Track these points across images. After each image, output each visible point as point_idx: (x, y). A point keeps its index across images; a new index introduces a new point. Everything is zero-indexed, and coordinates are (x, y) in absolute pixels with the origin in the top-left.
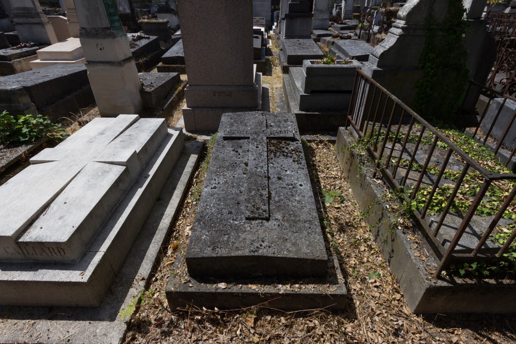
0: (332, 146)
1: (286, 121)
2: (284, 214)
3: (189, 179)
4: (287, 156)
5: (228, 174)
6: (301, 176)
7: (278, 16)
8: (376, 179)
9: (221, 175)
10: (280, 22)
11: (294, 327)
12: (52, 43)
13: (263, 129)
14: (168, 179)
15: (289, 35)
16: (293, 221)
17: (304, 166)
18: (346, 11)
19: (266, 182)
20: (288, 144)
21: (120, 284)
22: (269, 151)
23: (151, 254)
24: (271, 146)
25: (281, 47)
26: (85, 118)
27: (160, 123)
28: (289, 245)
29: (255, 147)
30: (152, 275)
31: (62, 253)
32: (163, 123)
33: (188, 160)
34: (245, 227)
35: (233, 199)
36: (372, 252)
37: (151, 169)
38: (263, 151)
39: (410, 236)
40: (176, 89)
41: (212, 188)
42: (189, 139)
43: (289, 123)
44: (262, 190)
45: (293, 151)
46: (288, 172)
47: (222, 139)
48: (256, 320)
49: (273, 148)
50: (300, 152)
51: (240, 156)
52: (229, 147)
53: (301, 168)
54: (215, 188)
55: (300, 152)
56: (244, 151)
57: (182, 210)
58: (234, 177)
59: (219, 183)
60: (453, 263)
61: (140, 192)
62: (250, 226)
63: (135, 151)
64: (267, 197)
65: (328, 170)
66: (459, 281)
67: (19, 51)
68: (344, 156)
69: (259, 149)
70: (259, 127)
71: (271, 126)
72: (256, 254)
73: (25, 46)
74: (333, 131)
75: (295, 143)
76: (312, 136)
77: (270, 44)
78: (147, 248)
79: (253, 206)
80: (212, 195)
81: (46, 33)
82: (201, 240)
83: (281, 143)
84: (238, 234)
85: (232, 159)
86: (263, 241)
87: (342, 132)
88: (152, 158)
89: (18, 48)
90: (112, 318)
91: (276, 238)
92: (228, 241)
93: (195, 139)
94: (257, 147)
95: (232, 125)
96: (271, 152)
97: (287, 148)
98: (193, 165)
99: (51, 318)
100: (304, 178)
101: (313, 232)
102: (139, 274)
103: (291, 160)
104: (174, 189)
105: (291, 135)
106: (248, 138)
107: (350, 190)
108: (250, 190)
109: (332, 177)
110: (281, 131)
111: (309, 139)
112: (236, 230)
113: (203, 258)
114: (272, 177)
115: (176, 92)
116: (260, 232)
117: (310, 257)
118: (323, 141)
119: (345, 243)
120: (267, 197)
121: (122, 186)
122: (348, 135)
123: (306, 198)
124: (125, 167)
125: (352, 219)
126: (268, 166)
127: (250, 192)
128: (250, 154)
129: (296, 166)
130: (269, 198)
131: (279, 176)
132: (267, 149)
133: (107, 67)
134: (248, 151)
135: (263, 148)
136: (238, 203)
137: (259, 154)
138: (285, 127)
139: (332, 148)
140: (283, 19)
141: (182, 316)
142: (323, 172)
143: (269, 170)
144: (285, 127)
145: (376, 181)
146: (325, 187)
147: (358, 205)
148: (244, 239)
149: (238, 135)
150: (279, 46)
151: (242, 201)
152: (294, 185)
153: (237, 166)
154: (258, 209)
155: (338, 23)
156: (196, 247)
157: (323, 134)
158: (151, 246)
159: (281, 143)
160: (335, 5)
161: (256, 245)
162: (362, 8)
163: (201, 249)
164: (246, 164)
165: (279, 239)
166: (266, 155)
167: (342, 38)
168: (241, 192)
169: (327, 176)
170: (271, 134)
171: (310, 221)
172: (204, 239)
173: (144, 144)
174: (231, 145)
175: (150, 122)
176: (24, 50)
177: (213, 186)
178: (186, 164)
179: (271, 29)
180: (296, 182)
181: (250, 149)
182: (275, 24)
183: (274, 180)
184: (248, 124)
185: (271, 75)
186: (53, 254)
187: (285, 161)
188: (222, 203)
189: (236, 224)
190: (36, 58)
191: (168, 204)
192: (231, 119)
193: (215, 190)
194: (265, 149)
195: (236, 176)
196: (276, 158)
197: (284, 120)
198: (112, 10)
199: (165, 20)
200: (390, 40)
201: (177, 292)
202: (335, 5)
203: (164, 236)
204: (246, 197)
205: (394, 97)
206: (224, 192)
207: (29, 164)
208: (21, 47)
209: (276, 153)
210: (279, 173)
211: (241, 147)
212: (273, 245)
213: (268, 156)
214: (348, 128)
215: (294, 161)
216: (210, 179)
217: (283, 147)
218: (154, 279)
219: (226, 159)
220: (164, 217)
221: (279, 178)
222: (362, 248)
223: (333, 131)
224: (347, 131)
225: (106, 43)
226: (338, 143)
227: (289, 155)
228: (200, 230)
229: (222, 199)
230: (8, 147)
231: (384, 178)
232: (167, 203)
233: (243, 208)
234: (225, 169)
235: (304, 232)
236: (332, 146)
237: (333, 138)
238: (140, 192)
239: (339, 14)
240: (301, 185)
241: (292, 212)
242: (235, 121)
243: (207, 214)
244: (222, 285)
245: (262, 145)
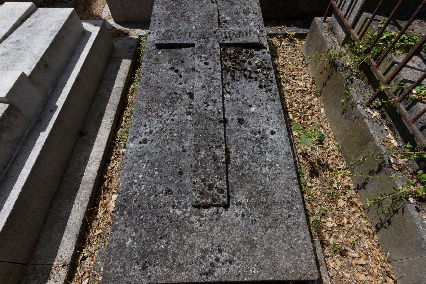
0: (298, 42)
1: (246, 12)
2: (250, 191)
3: (121, 99)
4: (250, 77)
5: (164, 114)
6: (273, 115)
8: (371, 109)
9: (153, 117)
14: (93, 100)
17: (275, 94)
19: (222, 131)
20: (252, 55)
21: (33, 276)
22: (225, 70)
23: (74, 223)
24: (226, 60)
27: (66, 17)
28: (259, 254)
29: (202, 64)
30: (76, 255)
32: (71, 16)
33: (118, 68)
34: (192, 222)
35: (173, 163)
36: (353, 209)
37: (59, 95)
38: (215, 70)
41: (140, 143)
43: (251, 16)
44: (217, 147)
45: (259, 67)
46: (253, 109)
47: (154, 47)
49: (229, 63)
50: (269, 69)
51: (180, 80)
53: (271, 99)
54: (145, 141)
55: (269, 69)
56: (187, 71)
57: (114, 145)
58: (173, 120)
59: (151, 132)
61: (43, 136)
62: (199, 220)
63: (23, 75)
64: (224, 163)
65: (294, 79)
69: (209, 66)
70: (208, 25)
71: (225, 22)
72: (210, 279)
75: (260, 52)
76: (273, 27)
78: (69, 213)
79: (204, 181)
80: (141, 156)
82: (125, 248)
83: (241, 53)
84: (181, 235)
85: (170, 85)
86: (220, 251)
87: (320, 26)
88: (61, 76)
91: (240, 242)
92: (166, 251)
93: (127, 34)
94: (206, 64)
95: (168, 20)
96: (228, 71)
97: (250, 63)
98: (126, 76)
100: (276, 119)
101: (294, 224)
102: (58, 257)
103: (255, 85)
104: (102, 115)
105: (256, 41)
106: (193, 45)
107: (322, 110)
108: (197, 149)
109: (300, 90)
110: (240, 32)
111: (271, 32)
112: (178, 227)
114: (229, 118)
116: (216, 230)
118: (289, 35)
119: (319, 193)
120: (224, 163)
122: (328, 33)
123: (282, 157)
124: (7, 105)
125: (326, 154)
126: (223, 99)
127: (198, 152)
128: (195, 75)
129: (263, 95)
130: (227, 162)
131: (241, 117)
132: (222, 65)
134: (193, 69)
135: (215, 65)
136: (181, 173)
137: (209, 76)
138: (246, 24)
139: (299, 44)
142: (288, 82)
143: (226, 106)
144: (246, 24)
145: (372, 113)
146: (292, 106)
147: (332, 133)
148: (192, 247)
149: (178, 41)
151: (186, 167)
152: (262, 133)
153: (178, 99)
154: (211, 187)
156: (116, 263)
157: (288, 25)
158: (73, 210)
159: (241, 53)
161: (210, 259)
163: (124, 267)
164: (191, 95)
165: (245, 243)
166: (220, 78)
168: (184, 151)
169: (293, 87)
170: (227, 37)
171: (288, 202)
172: (130, 247)
173: (39, 58)
174: (168, 58)
175: (50, 16)
177: (141, 139)
178: (116, 75)
180: (265, 126)
181: (197, 68)
183: (233, 124)
184: (192, 20)
188: (156, 173)
189: (178, 216)
191: (94, 141)
192: (167, 8)
193: (145, 146)
194: (219, 67)
195: (176, 118)
196: (235, 83)
197: (244, 10)
203: (90, 192)
206: (158, 150)
209: (234, 72)
210: (240, 112)
211: (183, 62)
212: (235, 258)
213: (222, 79)
214: (329, 18)
215: (261, 87)
216: (139, 125)
217: (244, 61)
218: (81, 257)
219: (160, 85)
220: (90, 162)
222: (341, 203)
224: (326, 24)
226: (309, 40)
227: (254, 75)
228: (123, 226)
229: (156, 164)
231: (383, 109)
232: (94, 138)
233: (187, 182)
234: (160, 105)
235: (282, 225)
236: (298, 42)
237: (301, 31)
238: (43, 136)
240: (273, 133)
241: (261, 188)
242: (173, 13)
243: (134, 194)
245: (214, 60)
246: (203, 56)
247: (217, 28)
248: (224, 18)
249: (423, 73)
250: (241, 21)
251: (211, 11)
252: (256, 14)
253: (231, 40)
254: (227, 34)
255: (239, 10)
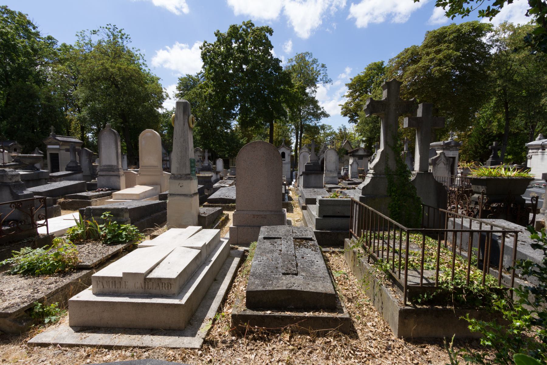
7: (296, 175)
10: (299, 178)
11: (316, 342)
12: (121, 188)
15: (306, 186)
16: (313, 277)
18: (352, 173)
25: (300, 195)
26: (155, 233)
31: (169, 288)
39: (390, 288)
40: (220, 218)
42: (232, 248)
46: (309, 255)
48: (291, 337)
52: (267, 243)
60: (412, 293)
66: (419, 307)
67: (97, 193)
68: (349, 254)
73: (102, 190)
74: (341, 244)
77: (291, 194)
81: (119, 182)
89: (96, 192)
90: (193, 335)
93: (237, 248)
99: (153, 335)
104: (225, 275)
106: (281, 238)
113: (257, 291)
115: (221, 220)
117: (324, 292)
121: (198, 262)
128: (282, 245)
129: (314, 252)
133: (182, 198)
135: (291, 243)
140: (301, 175)
141: (239, 336)
150: (298, 194)
155: (346, 180)
160: (342, 168)
162: (365, 171)
167: (348, 189)
176: (101, 193)
179: (290, 184)
182: (294, 180)
185: (292, 212)
186: (164, 288)
187: (306, 250)
190: (111, 198)
198: (193, 165)
199: (210, 175)
200: (367, 181)
201: (239, 315)
202: (342, 168)
204: (282, 264)
205: (370, 208)
207: (137, 248)
208: (99, 191)
221: (303, 258)
223: (341, 244)
225: (185, 183)
230: (110, 245)
237: (341, 250)
239: (346, 174)
244: (269, 312)
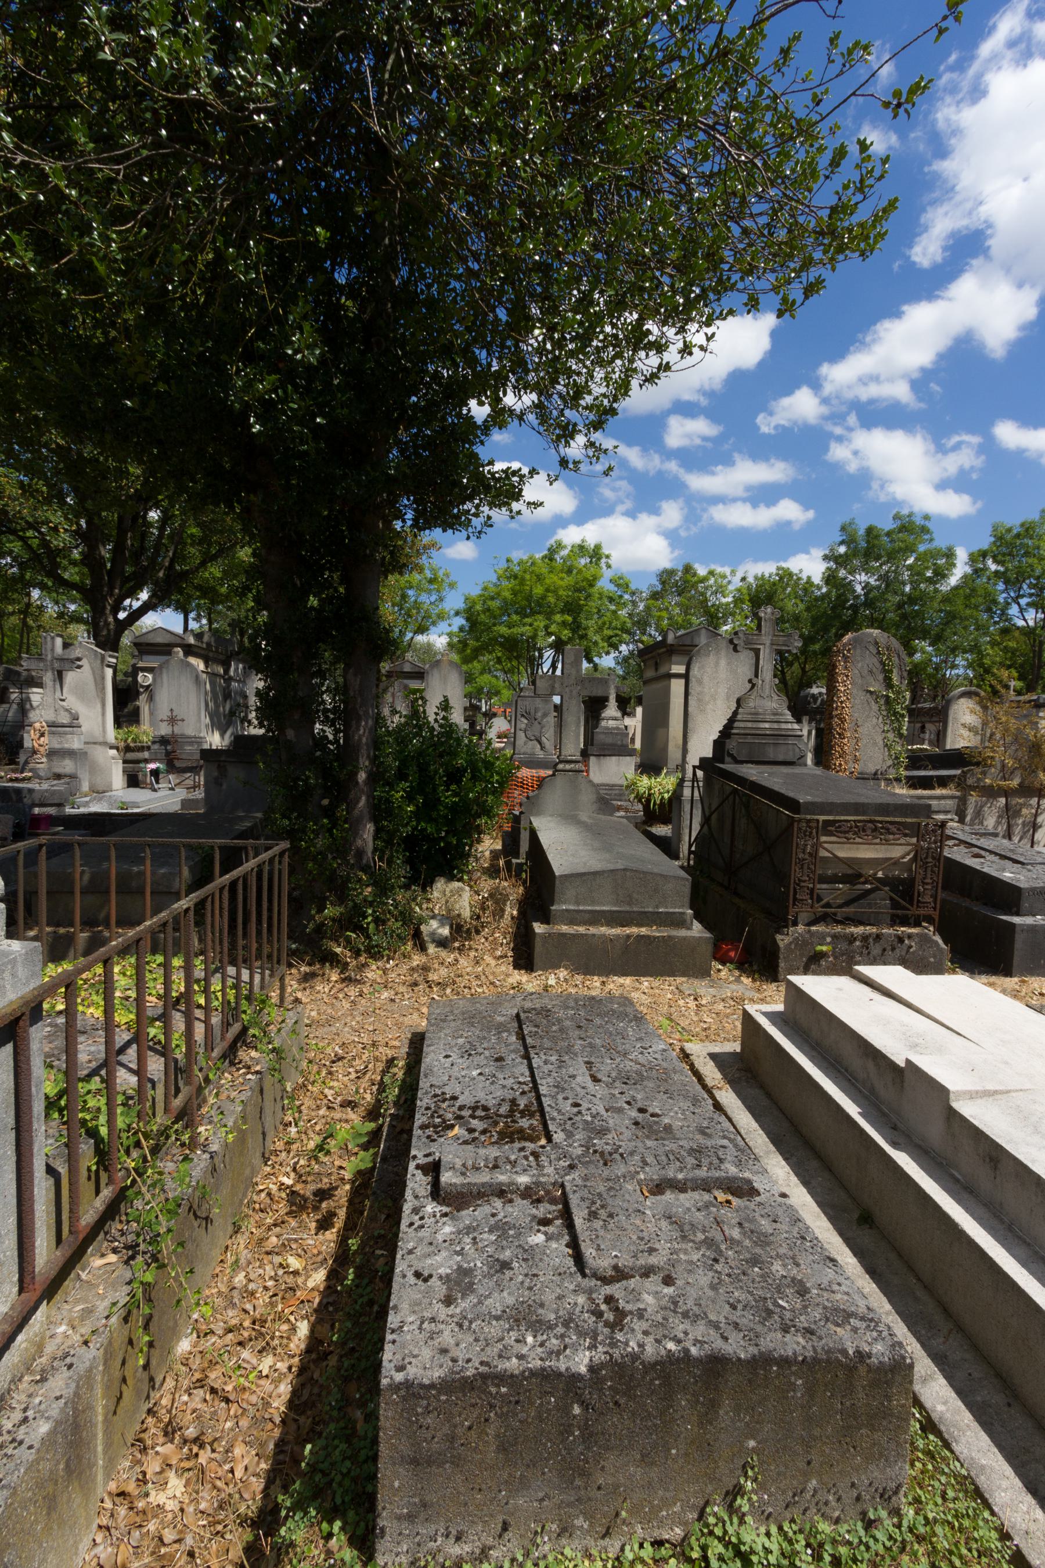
13: (575, 1175)
46: (475, 1073)
61: (852, 1109)
69: (570, 1101)
94: (576, 1105)
97: (471, 1131)
103: (465, 1099)
110: (496, 1167)
138: (469, 1230)
187: (481, 1096)
221: (500, 1059)
238: (852, 1109)
246: (589, 1119)
247: (568, 1178)
248: (549, 1238)
249: (118, 1046)
250: (485, 1236)
251: (602, 1233)
252: (418, 1275)
253: (522, 1149)
254: (533, 1164)
255: (492, 1284)
